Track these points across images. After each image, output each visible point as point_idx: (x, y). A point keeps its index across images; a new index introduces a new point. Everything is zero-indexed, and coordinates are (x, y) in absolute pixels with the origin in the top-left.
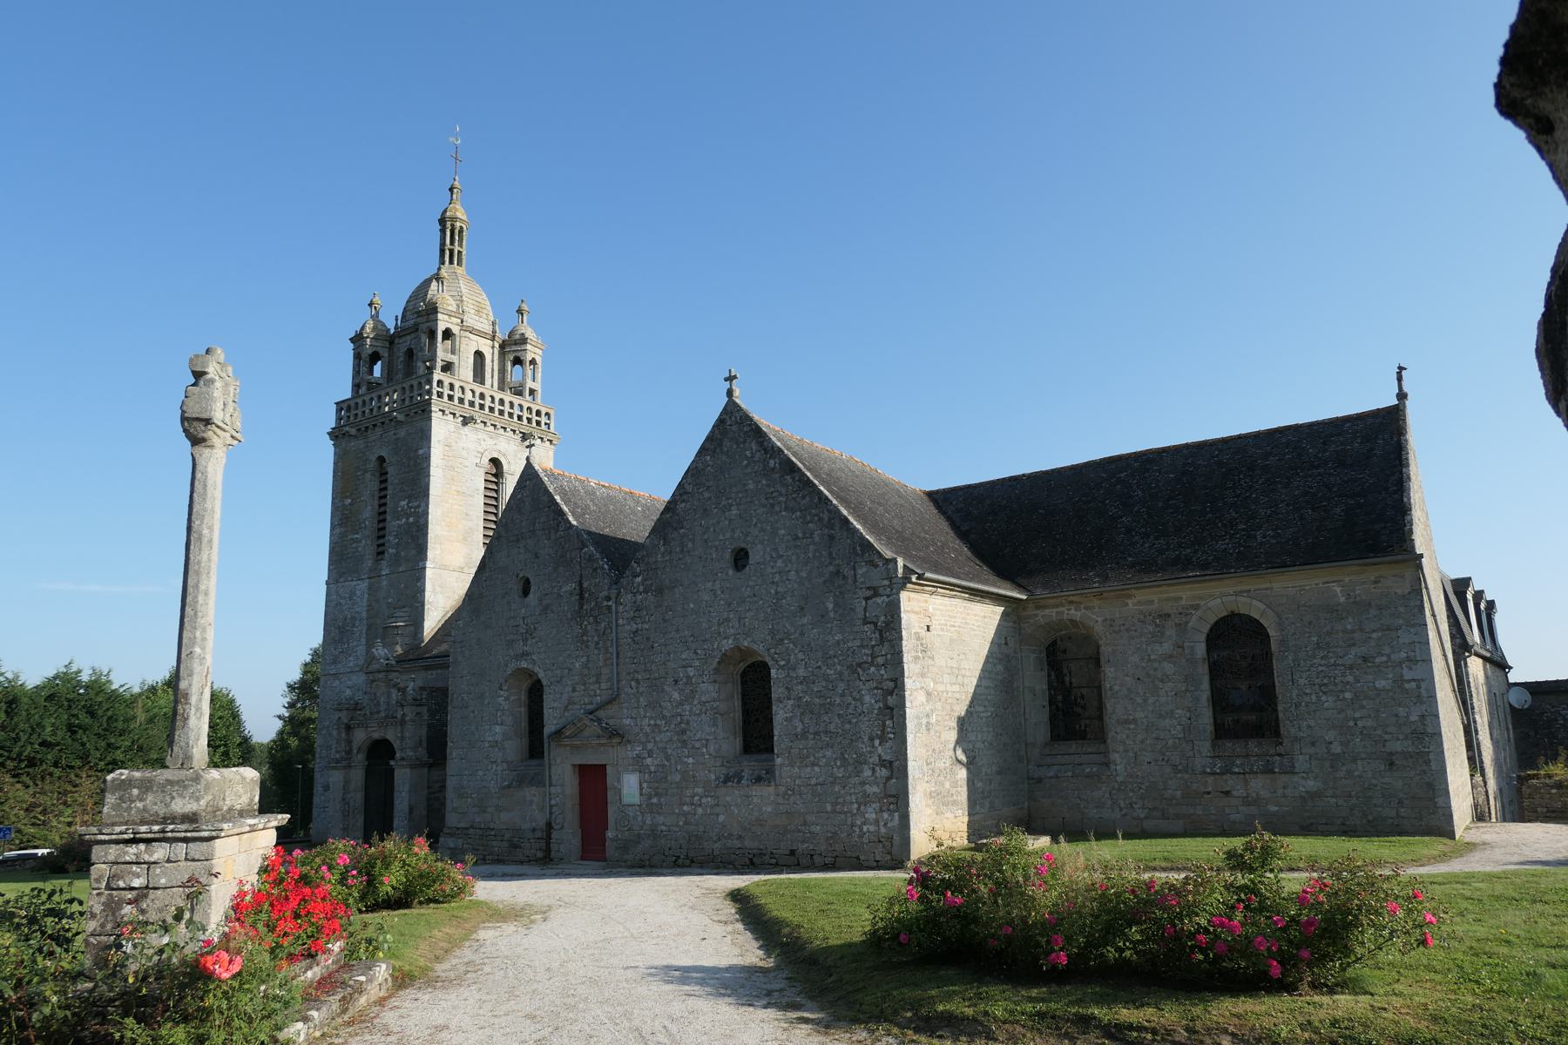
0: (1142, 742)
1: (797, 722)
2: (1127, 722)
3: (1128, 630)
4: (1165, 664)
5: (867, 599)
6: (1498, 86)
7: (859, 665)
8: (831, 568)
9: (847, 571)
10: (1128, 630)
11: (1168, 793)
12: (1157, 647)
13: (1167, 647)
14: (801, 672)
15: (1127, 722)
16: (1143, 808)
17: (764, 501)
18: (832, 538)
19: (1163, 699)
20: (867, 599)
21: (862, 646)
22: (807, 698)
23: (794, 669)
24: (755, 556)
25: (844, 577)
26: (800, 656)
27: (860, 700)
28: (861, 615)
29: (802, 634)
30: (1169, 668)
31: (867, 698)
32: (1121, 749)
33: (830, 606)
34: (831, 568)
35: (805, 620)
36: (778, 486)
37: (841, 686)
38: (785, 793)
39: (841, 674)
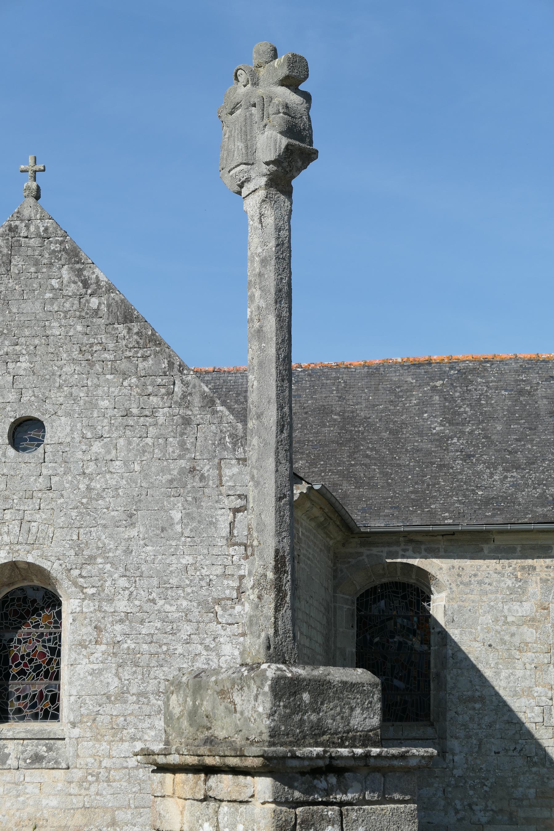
0: (490, 726)
1: (109, 677)
2: (472, 699)
3: (480, 583)
4: (525, 628)
5: (236, 511)
6: (305, 168)
7: (218, 601)
8: (183, 463)
9: (206, 468)
10: (480, 583)
11: (518, 792)
12: (516, 606)
13: (527, 608)
14: (122, 605)
15: (472, 699)
16: (485, 810)
17: (75, 354)
18: (187, 421)
19: (519, 673)
20: (236, 511)
21: (224, 575)
22: (130, 644)
23: (110, 600)
24: (57, 431)
25: (202, 478)
26: (123, 582)
27: (217, 651)
28: (225, 532)
29: (128, 551)
30: (529, 634)
31: (227, 649)
32: (462, 734)
33: (177, 515)
34: (183, 463)
35: (133, 533)
36: (103, 338)
37: (188, 628)
38: (84, 780)
39: (187, 612)
